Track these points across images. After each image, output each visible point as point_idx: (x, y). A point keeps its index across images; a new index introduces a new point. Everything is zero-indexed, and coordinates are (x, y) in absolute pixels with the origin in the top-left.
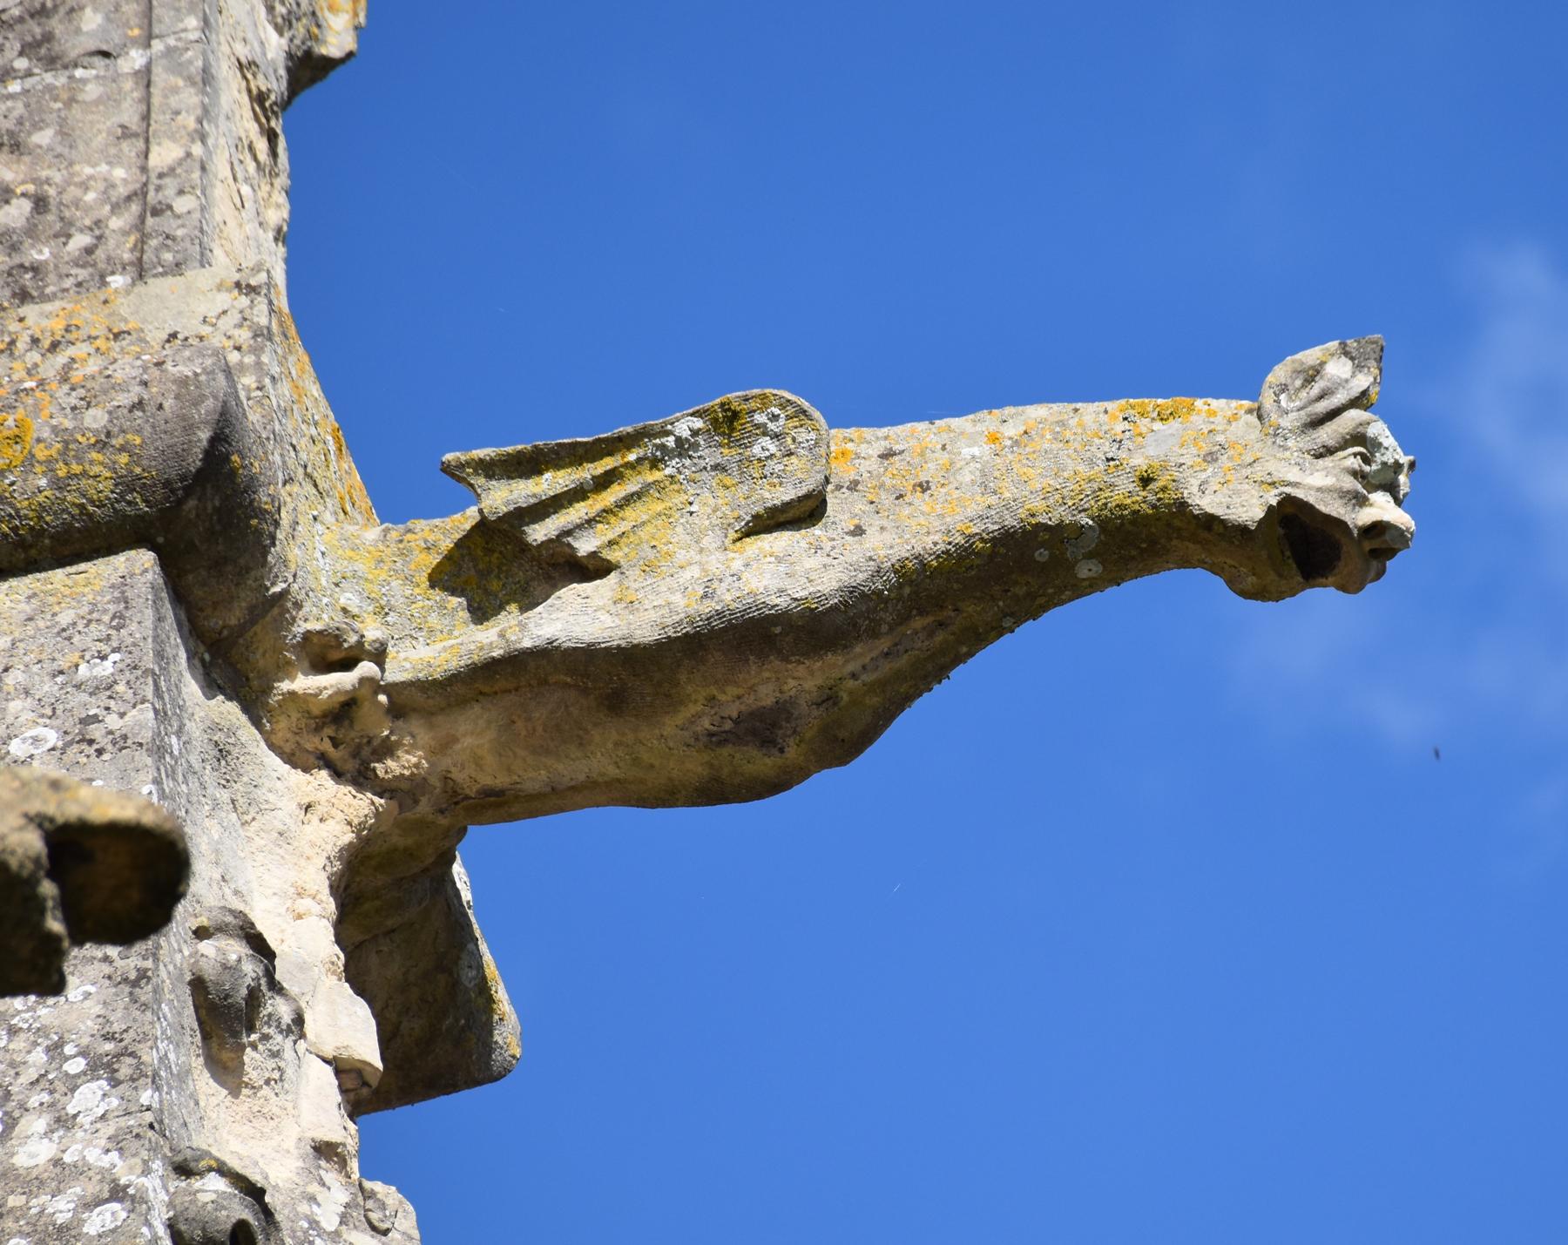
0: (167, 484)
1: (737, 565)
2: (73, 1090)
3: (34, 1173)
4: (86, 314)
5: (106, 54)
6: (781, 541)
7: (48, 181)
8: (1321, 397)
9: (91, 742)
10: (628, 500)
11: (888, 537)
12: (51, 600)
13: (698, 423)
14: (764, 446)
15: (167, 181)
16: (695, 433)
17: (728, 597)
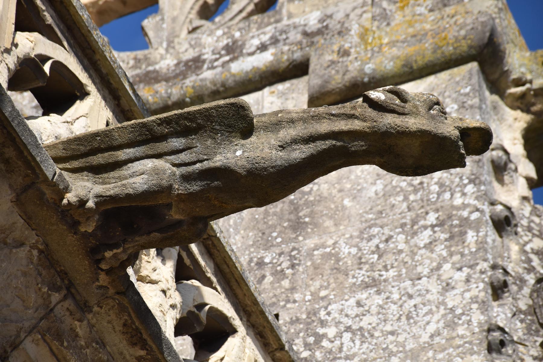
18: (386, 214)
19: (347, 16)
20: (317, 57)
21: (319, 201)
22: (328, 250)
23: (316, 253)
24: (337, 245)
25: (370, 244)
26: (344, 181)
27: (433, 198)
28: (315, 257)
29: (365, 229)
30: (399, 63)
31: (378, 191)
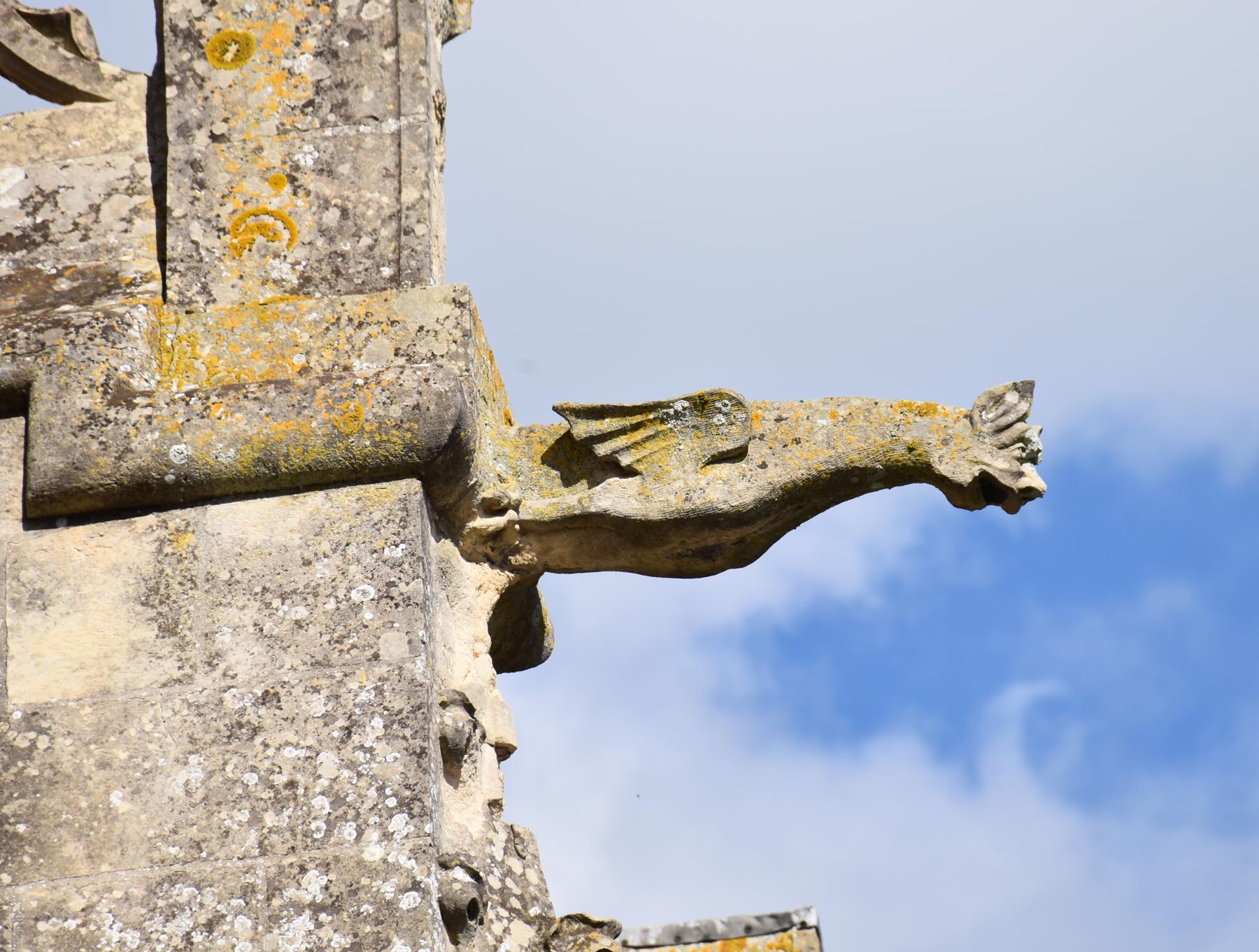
0: (429, 449)
1: (703, 483)
2: (391, 816)
3: (374, 866)
4: (376, 306)
5: (376, 119)
6: (724, 470)
7: (348, 198)
8: (1003, 414)
9: (392, 598)
10: (648, 438)
11: (779, 470)
12: (369, 503)
13: (686, 404)
14: (719, 419)
15: (411, 212)
16: (684, 409)
17: (699, 502)
18: (210, 854)
19: (96, 209)
20: (54, 390)
21: (52, 783)
22: (72, 924)
23: (42, 926)
24: (93, 916)
25: (170, 927)
26: (112, 739)
27: (318, 830)
28: (41, 939)
29: (160, 884)
30: (249, 455)
31: (193, 785)
